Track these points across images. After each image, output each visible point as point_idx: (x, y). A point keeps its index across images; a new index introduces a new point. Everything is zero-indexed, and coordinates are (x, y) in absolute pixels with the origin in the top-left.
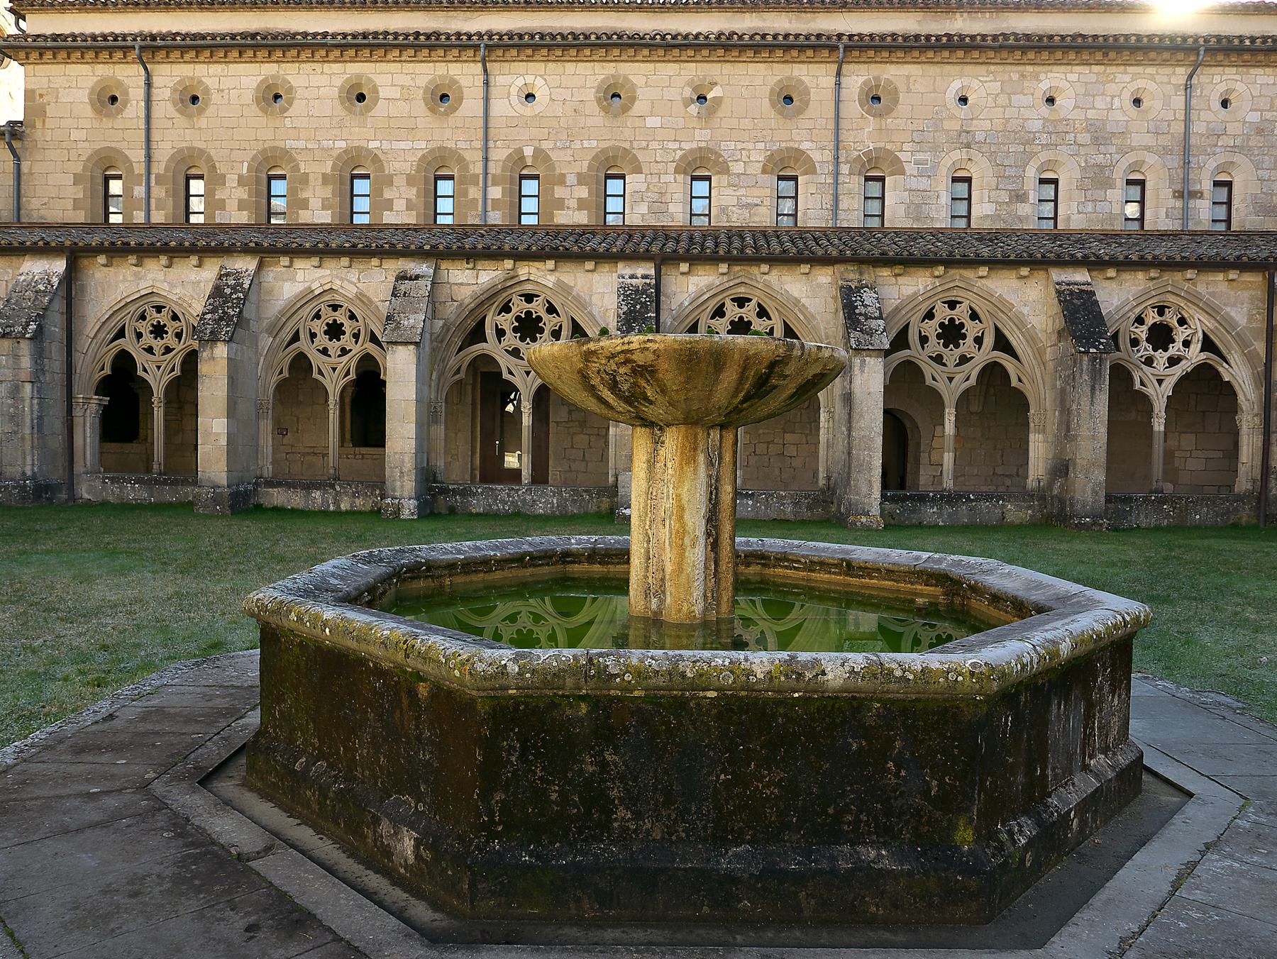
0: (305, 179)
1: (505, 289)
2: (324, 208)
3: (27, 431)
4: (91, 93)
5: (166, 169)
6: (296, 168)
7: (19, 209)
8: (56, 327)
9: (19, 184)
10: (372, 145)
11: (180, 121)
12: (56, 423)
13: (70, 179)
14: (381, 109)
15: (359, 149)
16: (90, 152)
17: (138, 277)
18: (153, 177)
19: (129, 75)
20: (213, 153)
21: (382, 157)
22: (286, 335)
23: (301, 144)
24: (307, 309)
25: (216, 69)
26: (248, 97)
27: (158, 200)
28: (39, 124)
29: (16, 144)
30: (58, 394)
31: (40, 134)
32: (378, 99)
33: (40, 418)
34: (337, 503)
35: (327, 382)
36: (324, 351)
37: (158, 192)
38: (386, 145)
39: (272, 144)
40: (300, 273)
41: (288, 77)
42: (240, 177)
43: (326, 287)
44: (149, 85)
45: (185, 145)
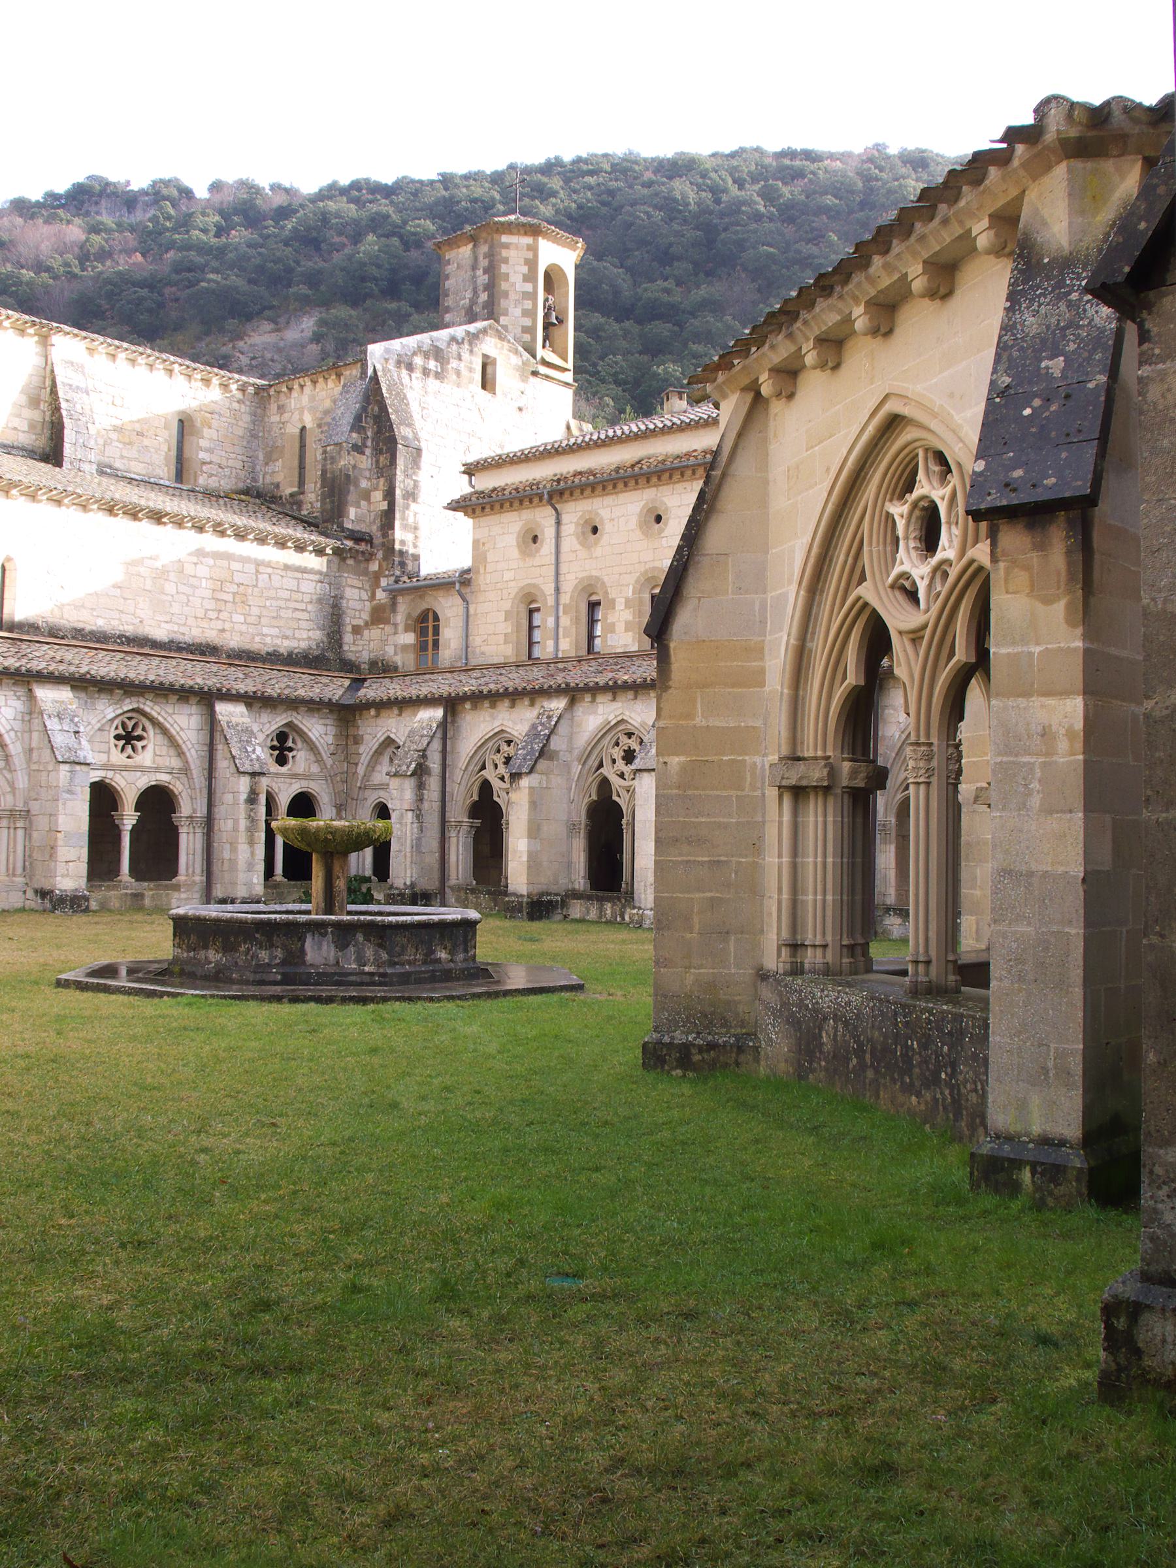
3: (408, 850)
4: (518, 538)
7: (467, 647)
8: (434, 764)
9: (467, 625)
11: (583, 553)
12: (432, 841)
16: (516, 590)
17: (493, 718)
18: (561, 608)
19: (543, 517)
20: (606, 579)
22: (593, 762)
26: (634, 521)
27: (565, 628)
28: (482, 571)
30: (433, 820)
31: (483, 580)
33: (419, 839)
37: (565, 621)
39: (651, 565)
43: (619, 718)
44: (558, 523)
45: (584, 574)
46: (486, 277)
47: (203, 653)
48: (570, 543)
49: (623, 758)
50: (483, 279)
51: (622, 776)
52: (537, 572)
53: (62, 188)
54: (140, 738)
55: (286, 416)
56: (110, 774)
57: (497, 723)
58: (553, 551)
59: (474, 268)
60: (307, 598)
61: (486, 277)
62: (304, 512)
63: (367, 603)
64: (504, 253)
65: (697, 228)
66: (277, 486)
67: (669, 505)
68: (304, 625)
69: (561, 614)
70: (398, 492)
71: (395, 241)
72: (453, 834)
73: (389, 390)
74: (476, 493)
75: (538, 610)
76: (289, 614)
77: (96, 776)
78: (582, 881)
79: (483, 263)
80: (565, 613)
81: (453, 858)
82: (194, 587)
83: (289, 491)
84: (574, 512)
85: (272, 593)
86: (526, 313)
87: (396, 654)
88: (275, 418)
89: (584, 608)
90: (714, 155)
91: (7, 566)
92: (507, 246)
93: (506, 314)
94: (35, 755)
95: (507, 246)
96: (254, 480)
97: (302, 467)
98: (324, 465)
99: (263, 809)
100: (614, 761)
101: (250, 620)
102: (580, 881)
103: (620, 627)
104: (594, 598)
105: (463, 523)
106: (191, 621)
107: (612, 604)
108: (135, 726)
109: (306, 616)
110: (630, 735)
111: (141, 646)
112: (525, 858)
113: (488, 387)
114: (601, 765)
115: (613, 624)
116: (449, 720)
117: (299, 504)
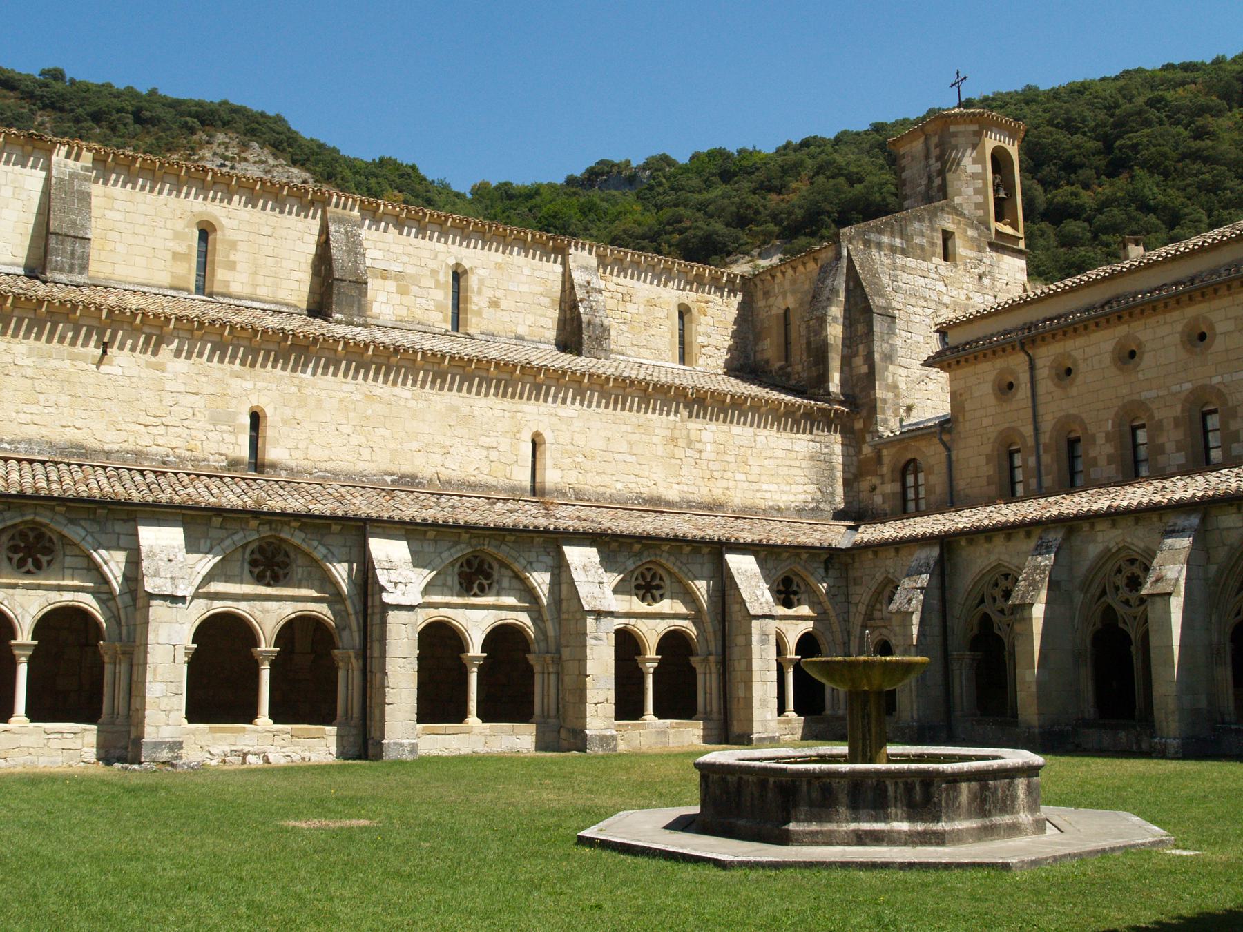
0: (1159, 426)
1: (1100, 568)
2: (1178, 450)
5: (1051, 438)
6: (1151, 417)
10: (1216, 380)
13: (983, 460)
14: (1219, 345)
15: (1203, 387)
17: (989, 552)
20: (1084, 416)
21: (1225, 391)
22: (1095, 590)
23: (1153, 394)
24: (1109, 566)
25: (1081, 341)
26: (1107, 360)
28: (961, 419)
29: (945, 438)
32: (1215, 335)
34: (1138, 743)
35: (1129, 629)
36: (1127, 602)
37: (1046, 459)
38: (1227, 378)
40: (1100, 534)
41: (1138, 335)
42: (1107, 434)
44: (1032, 367)
45: (1063, 413)
46: (939, 164)
47: (711, 509)
48: (1046, 385)
49: (1127, 585)
50: (935, 166)
51: (1127, 602)
52: (1017, 414)
53: (578, 171)
54: (659, 587)
55: (771, 300)
56: (632, 621)
57: (993, 558)
58: (1029, 394)
59: (927, 157)
60: (800, 456)
61: (939, 164)
62: (793, 382)
63: (855, 459)
64: (953, 141)
65: (1096, 139)
66: (767, 362)
67: (1143, 338)
68: (800, 480)
69: (1041, 452)
70: (877, 356)
71: (842, 180)
72: (956, 666)
73: (862, 267)
74: (950, 349)
75: (1018, 451)
76: (785, 471)
77: (619, 623)
78: (1092, 710)
79: (935, 152)
80: (1045, 452)
81: (957, 691)
82: (701, 452)
83: (777, 365)
84: (1046, 355)
85: (769, 453)
86: (977, 191)
87: (884, 502)
88: (761, 303)
89: (1064, 445)
90: (1103, 79)
91: (537, 440)
92: (955, 135)
93: (960, 194)
94: (564, 605)
95: (955, 135)
96: (747, 357)
97: (787, 343)
98: (808, 338)
99: (774, 650)
100: (1117, 589)
101: (751, 478)
102: (1090, 711)
103: (1102, 461)
104: (1073, 435)
105: (940, 377)
106: (699, 482)
107: (1093, 439)
108: (653, 577)
109: (801, 472)
110: (1132, 561)
111: (656, 505)
112: (1034, 688)
113: (950, 257)
114: (1104, 593)
115: (1095, 459)
116: (946, 556)
117: (788, 376)
